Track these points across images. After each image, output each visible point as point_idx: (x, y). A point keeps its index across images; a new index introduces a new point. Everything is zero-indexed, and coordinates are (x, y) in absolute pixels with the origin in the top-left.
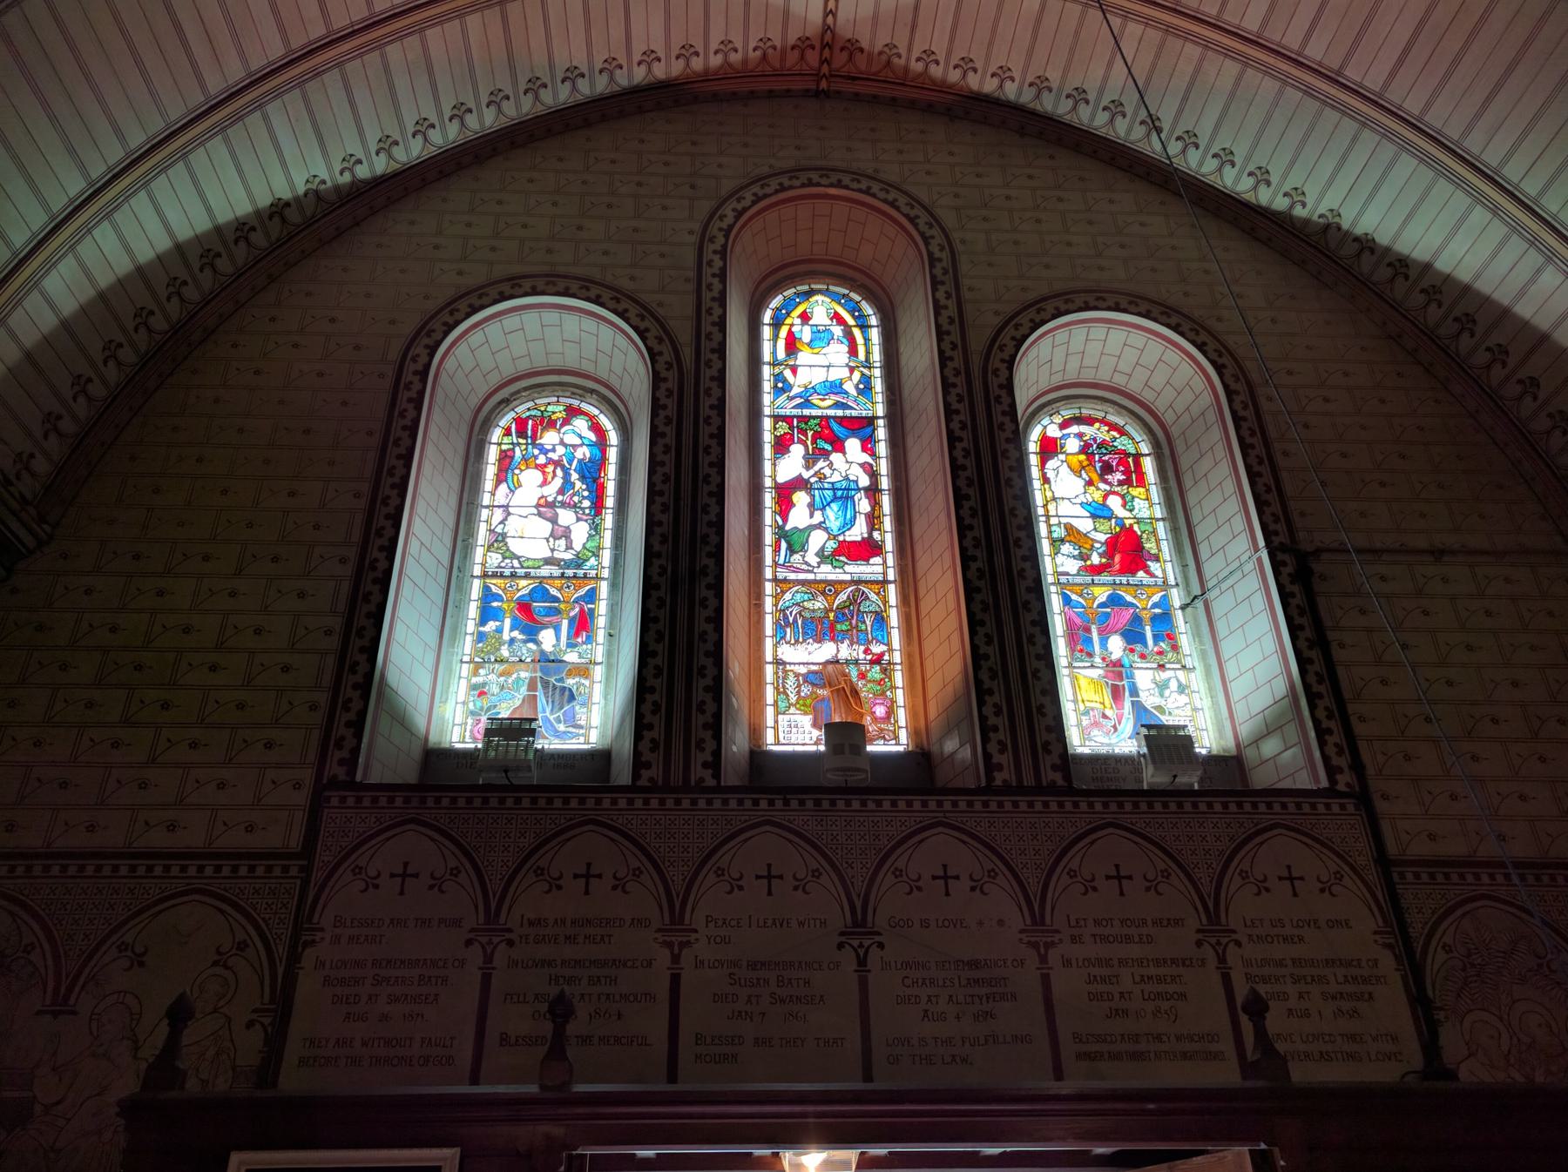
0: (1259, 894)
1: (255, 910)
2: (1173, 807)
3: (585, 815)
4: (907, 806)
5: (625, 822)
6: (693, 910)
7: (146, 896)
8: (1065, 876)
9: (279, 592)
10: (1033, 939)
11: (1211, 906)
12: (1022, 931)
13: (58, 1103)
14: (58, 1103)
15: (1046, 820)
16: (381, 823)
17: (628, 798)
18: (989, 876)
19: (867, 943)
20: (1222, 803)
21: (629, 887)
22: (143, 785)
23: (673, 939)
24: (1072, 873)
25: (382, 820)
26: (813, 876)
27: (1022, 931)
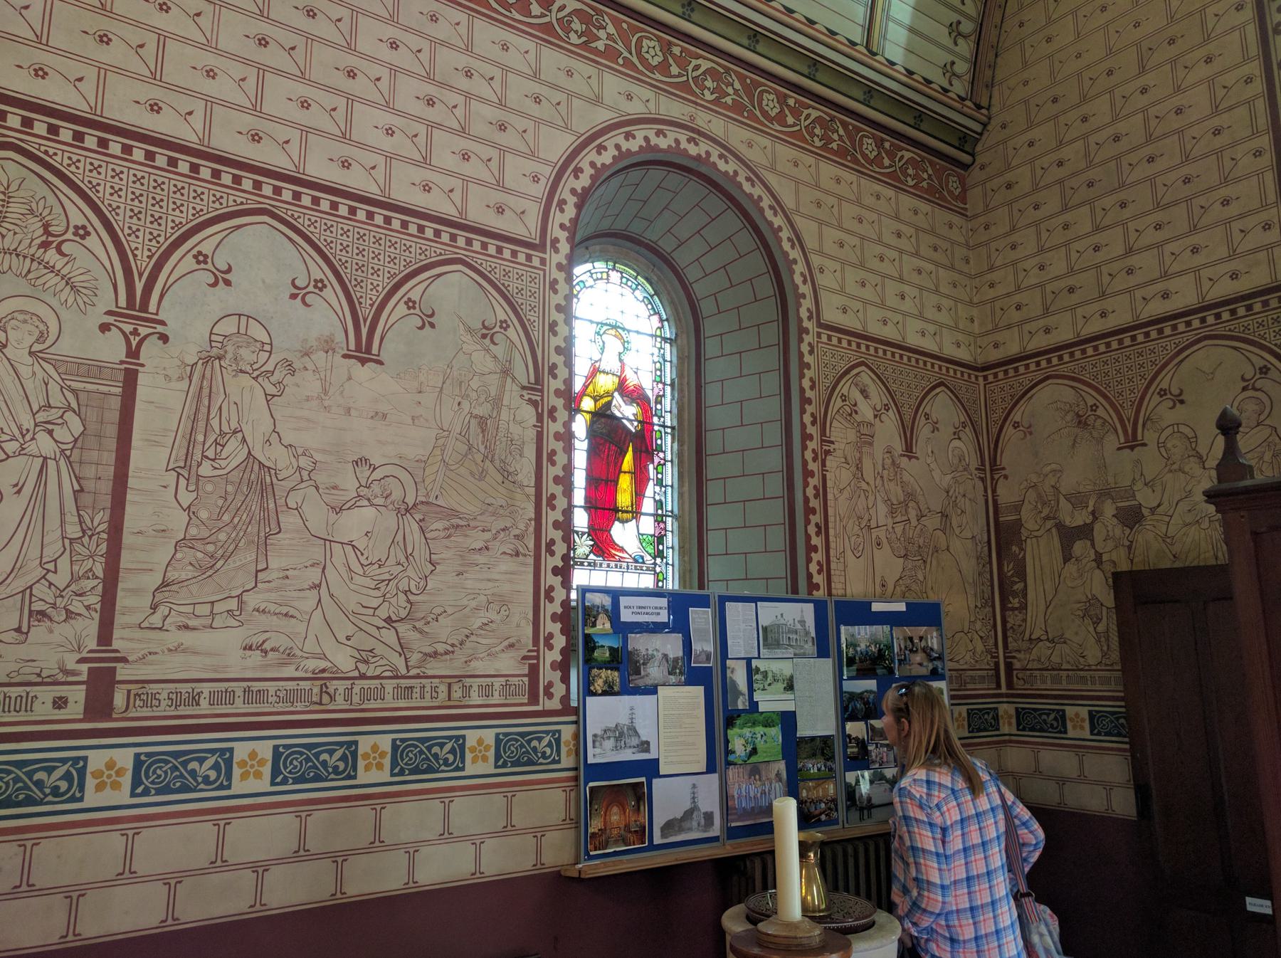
1: (1265, 339)
7: (1165, 352)
8: (402, 304)
9: (1186, 67)
13: (1159, 506)
14: (1159, 506)
19: (143, 331)
20: (350, 207)
22: (1130, 271)
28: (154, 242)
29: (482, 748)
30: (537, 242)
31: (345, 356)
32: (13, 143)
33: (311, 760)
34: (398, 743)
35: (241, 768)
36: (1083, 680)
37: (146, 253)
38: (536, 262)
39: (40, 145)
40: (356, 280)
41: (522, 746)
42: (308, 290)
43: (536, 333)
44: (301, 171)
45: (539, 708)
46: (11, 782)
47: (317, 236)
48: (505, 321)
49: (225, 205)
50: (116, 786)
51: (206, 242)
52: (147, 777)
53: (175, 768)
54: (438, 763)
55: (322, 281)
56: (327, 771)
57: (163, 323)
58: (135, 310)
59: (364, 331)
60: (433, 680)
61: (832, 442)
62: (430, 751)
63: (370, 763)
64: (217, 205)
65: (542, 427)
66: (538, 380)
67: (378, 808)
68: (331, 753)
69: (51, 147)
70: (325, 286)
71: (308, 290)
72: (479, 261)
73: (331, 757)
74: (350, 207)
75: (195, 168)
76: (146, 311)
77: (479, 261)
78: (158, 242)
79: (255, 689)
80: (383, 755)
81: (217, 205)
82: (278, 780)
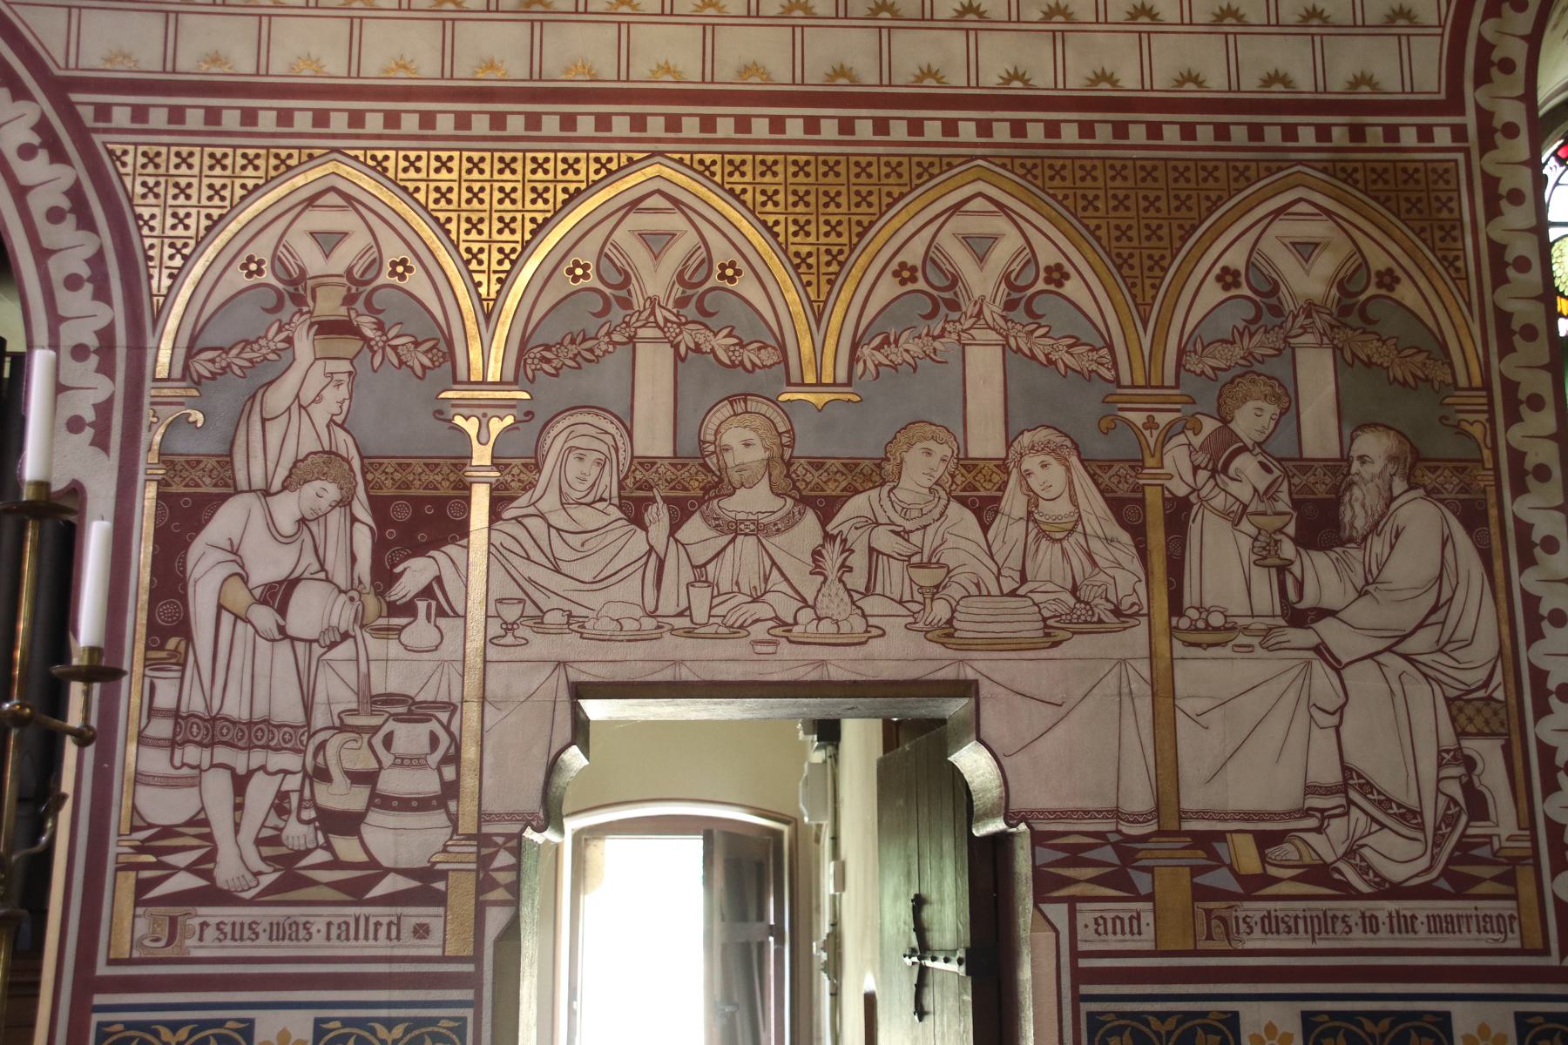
18: (1048, 281)
42: (1250, 294)
48: (1059, 267)
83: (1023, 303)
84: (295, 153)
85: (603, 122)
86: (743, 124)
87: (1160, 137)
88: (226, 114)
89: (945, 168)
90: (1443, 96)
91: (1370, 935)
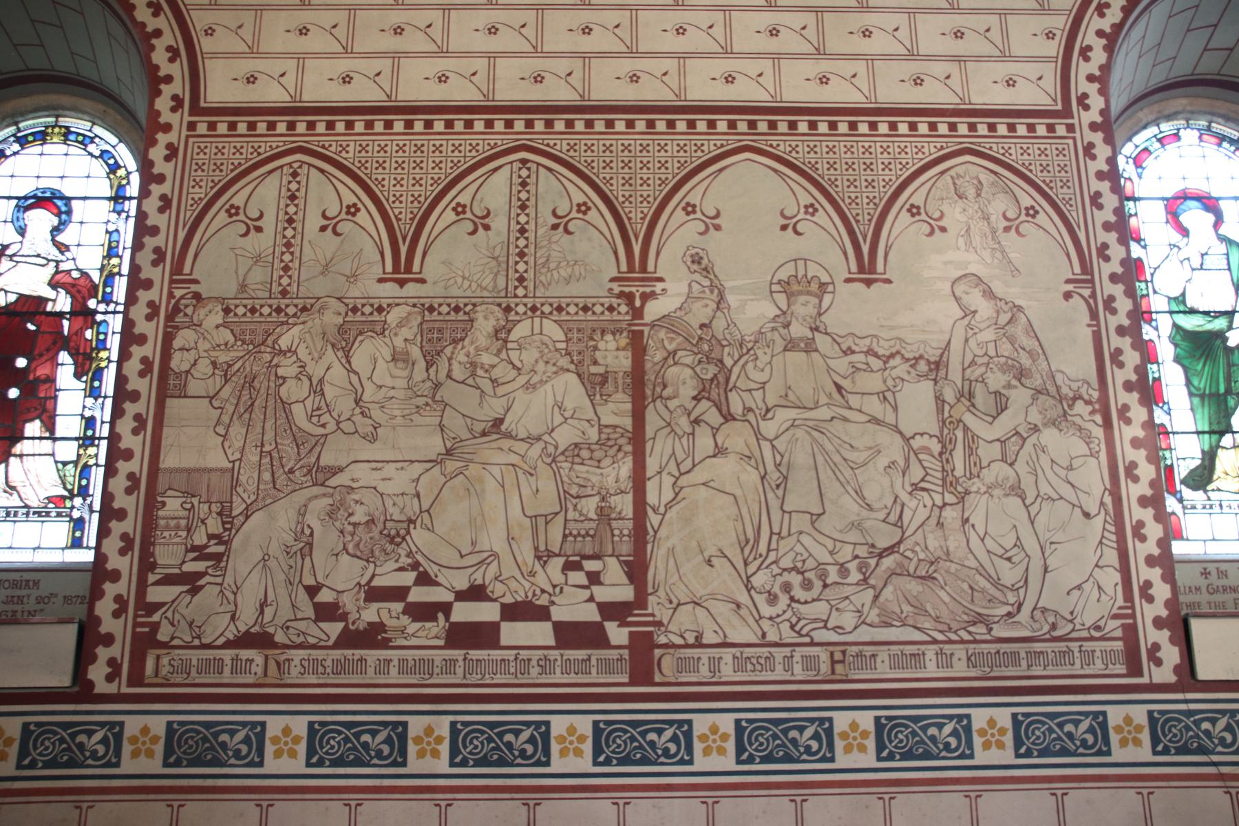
0: (931, 233)
2: (1022, 130)
3: (961, 143)
4: (950, 130)
5: (789, 149)
6: (658, 254)
8: (679, 211)
10: (627, 290)
11: (865, 249)
12: (613, 280)
15: (626, 143)
16: (259, 154)
17: (385, 120)
18: (1027, 215)
20: (1008, 124)
21: (1024, 228)
23: (633, 289)
24: (914, 210)
25: (261, 150)
26: (806, 213)
27: (613, 280)
28: (645, 204)
29: (995, 731)
30: (1059, 107)
31: (848, 281)
32: (300, 146)
33: (917, 735)
34: (602, 726)
35: (704, 742)
36: (1014, 658)
37: (867, 217)
38: (1061, 130)
39: (543, 139)
40: (850, 197)
41: (775, 736)
42: (571, 216)
43: (1074, 214)
44: (967, 102)
45: (1145, 680)
46: (57, 743)
47: (577, 159)
48: (1032, 207)
49: (927, 154)
50: (435, 754)
51: (693, 193)
52: (751, 744)
53: (490, 740)
54: (369, 755)
55: (1032, 207)
56: (369, 755)
57: (196, 282)
58: (865, 273)
59: (637, 249)
60: (892, 647)
61: (661, 280)
62: (358, 739)
63: (709, 746)
64: (920, 155)
65: (1098, 325)
66: (1086, 267)
67: (176, 804)
68: (374, 733)
69: (551, 139)
70: (1037, 212)
71: (571, 216)
72: (988, 146)
73: (659, 736)
74: (1008, 124)
75: (691, 124)
76: (875, 273)
77: (552, 143)
78: (649, 202)
79: (244, 658)
80: (297, 740)
81: (920, 155)
82: (26, 762)
83: (330, 228)
84: (263, 145)
85: (873, 126)
86: (953, 127)
87: (936, 130)
88: (577, 123)
89: (268, 149)
90: (202, 104)
91: (566, 675)
